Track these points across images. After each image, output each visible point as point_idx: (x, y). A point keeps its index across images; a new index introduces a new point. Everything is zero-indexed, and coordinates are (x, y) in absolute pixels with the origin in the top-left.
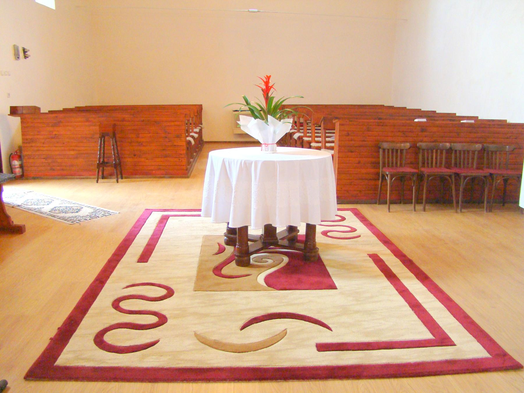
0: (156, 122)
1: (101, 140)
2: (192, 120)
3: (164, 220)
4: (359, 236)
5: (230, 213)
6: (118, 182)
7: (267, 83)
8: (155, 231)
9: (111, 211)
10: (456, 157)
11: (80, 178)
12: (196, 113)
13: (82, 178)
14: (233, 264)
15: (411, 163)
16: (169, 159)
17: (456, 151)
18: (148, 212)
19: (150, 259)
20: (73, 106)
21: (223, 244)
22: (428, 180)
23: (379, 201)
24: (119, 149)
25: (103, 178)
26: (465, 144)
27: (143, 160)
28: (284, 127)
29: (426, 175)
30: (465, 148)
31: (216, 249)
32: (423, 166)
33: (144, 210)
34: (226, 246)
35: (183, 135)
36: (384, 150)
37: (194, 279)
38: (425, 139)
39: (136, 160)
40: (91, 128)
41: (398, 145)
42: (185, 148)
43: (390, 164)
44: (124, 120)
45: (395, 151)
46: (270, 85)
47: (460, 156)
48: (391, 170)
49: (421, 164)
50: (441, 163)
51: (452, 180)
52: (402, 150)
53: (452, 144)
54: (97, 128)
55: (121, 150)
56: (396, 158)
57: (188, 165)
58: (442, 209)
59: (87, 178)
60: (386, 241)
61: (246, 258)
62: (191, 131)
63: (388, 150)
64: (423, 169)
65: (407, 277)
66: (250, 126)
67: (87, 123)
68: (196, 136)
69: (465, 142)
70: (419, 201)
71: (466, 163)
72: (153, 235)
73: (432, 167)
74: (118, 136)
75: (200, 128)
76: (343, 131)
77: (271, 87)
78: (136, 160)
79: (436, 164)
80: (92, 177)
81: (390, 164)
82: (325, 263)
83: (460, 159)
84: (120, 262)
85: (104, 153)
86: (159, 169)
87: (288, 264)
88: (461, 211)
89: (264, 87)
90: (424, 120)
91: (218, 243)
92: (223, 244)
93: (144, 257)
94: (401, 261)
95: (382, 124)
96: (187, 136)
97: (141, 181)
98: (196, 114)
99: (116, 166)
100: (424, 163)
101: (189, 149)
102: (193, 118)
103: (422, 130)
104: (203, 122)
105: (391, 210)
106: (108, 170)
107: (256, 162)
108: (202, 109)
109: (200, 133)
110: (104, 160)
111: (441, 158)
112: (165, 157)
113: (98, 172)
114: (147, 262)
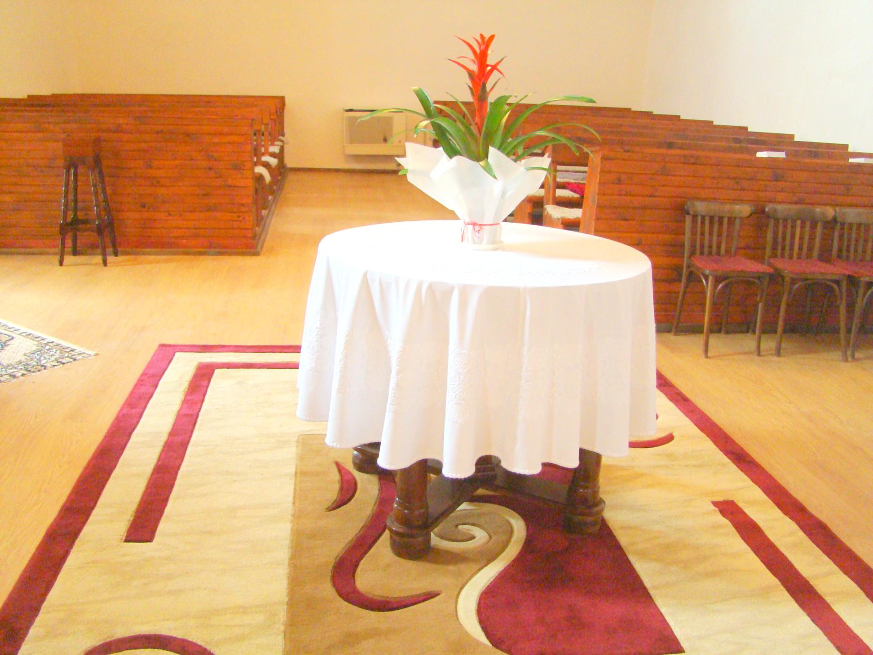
0: (188, 135)
1: (68, 171)
2: (266, 129)
3: (203, 377)
4: (669, 438)
5: (383, 422)
6: (105, 263)
7: (481, 58)
8: (180, 416)
9: (79, 349)
10: (841, 236)
11: (25, 254)
12: (270, 115)
13: (29, 254)
14: (383, 546)
15: (747, 247)
16: (218, 215)
17: (843, 224)
18: (166, 354)
19: (162, 526)
20: (20, 93)
21: (350, 467)
22: (791, 289)
23: (676, 328)
24: (109, 190)
25: (75, 253)
26: (861, 210)
27: (162, 216)
28: (526, 177)
29: (787, 279)
30: (864, 220)
31: (332, 492)
32: (774, 256)
33: (154, 347)
34: (357, 474)
35: (248, 165)
36: (695, 217)
37: (282, 615)
38: (780, 197)
39: (146, 215)
40: (45, 146)
41: (727, 207)
42: (251, 191)
43: (706, 250)
44: (119, 130)
45: (716, 219)
46: (491, 61)
47: (849, 234)
48: (715, 266)
49: (782, 253)
50: (810, 249)
51: (840, 291)
52: (731, 221)
53: (837, 209)
54: (60, 145)
55: (114, 193)
56: (720, 235)
57: (258, 225)
58: (810, 351)
59: (41, 254)
60: (741, 458)
61: (420, 539)
62: (263, 150)
63: (703, 217)
64: (779, 264)
65: (753, 503)
66: (430, 169)
67: (40, 135)
68: (273, 162)
69: (865, 206)
70: (769, 328)
71: (860, 249)
72: (173, 433)
73: (791, 257)
74: (105, 163)
75: (280, 143)
76: (610, 172)
77: (494, 67)
78: (146, 215)
79: (800, 249)
80: (53, 250)
81: (706, 250)
82: (623, 540)
83: (849, 240)
84: (78, 542)
85: (76, 201)
86: (196, 236)
87: (528, 544)
88: (853, 356)
89: (474, 67)
90: (781, 155)
91: (338, 465)
92: (350, 467)
93: (143, 526)
94: (802, 528)
95: (692, 160)
96: (256, 164)
97: (158, 262)
98: (274, 117)
99: (100, 231)
100: (774, 248)
101: (260, 190)
102: (268, 124)
103: (777, 178)
104: (286, 130)
105: (709, 354)
106: (86, 237)
107: (465, 291)
108: (284, 104)
109: (280, 156)
110: (75, 215)
111: (812, 238)
112: (208, 211)
113: (63, 244)
114: (150, 540)
